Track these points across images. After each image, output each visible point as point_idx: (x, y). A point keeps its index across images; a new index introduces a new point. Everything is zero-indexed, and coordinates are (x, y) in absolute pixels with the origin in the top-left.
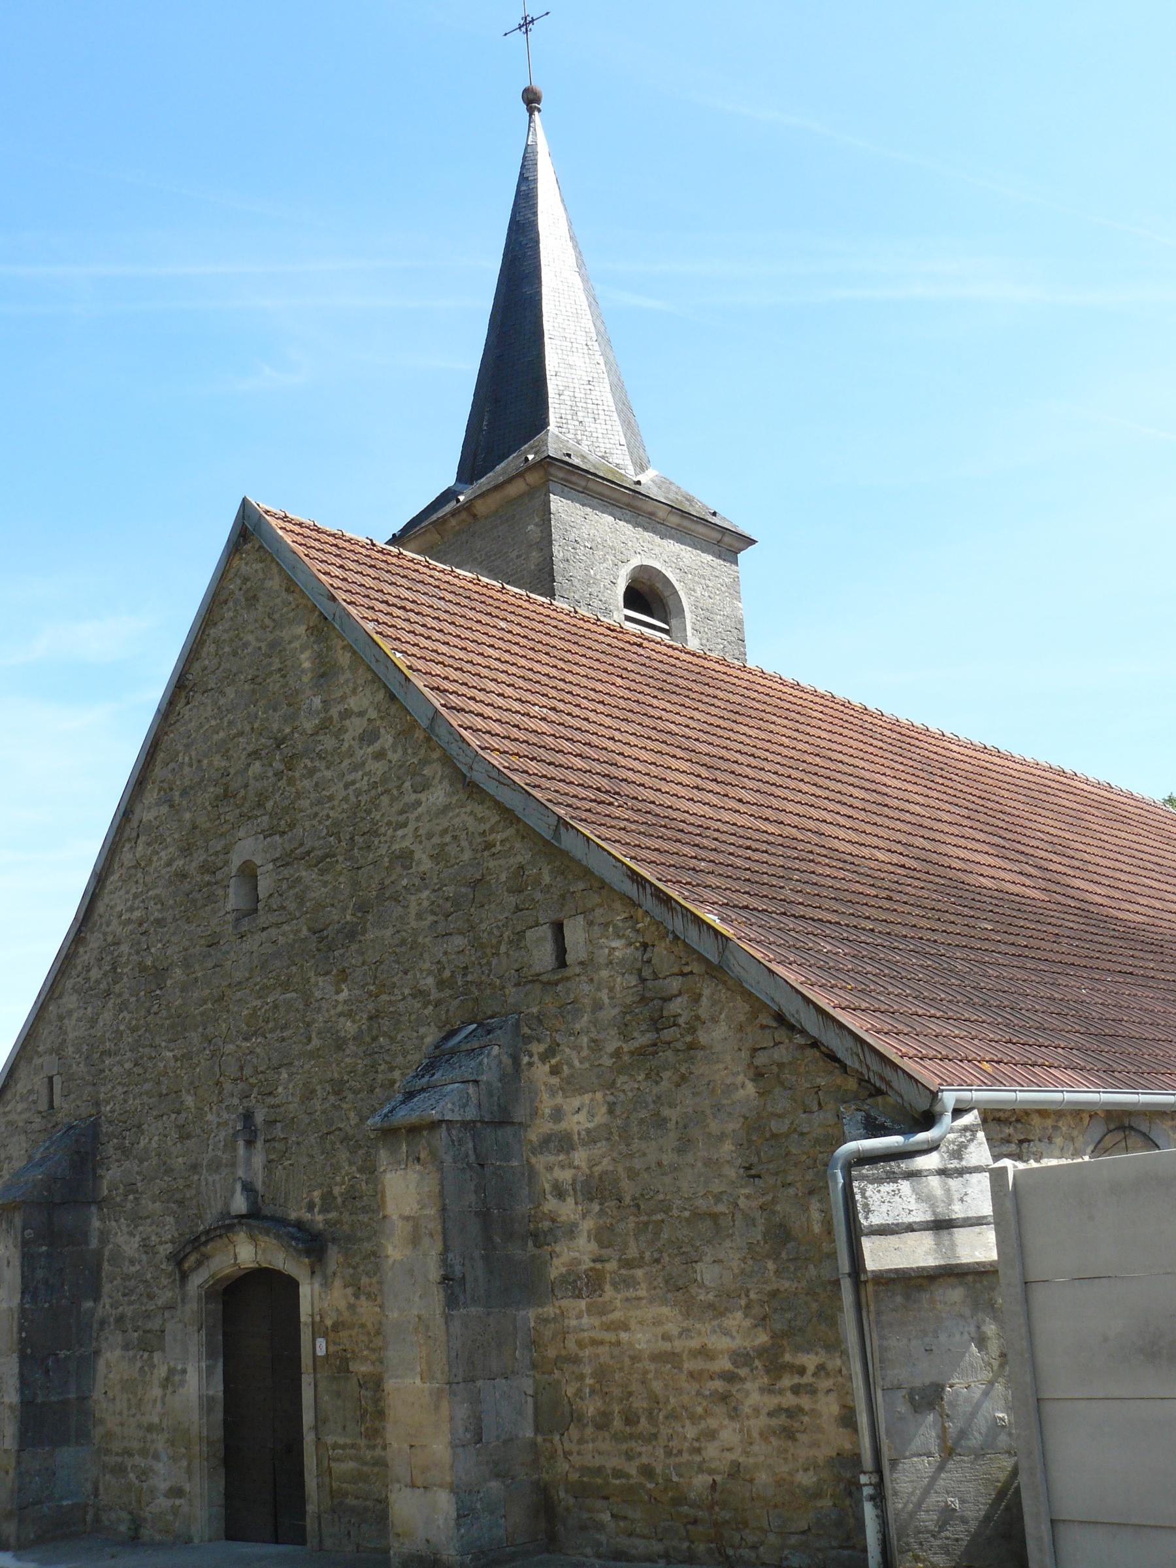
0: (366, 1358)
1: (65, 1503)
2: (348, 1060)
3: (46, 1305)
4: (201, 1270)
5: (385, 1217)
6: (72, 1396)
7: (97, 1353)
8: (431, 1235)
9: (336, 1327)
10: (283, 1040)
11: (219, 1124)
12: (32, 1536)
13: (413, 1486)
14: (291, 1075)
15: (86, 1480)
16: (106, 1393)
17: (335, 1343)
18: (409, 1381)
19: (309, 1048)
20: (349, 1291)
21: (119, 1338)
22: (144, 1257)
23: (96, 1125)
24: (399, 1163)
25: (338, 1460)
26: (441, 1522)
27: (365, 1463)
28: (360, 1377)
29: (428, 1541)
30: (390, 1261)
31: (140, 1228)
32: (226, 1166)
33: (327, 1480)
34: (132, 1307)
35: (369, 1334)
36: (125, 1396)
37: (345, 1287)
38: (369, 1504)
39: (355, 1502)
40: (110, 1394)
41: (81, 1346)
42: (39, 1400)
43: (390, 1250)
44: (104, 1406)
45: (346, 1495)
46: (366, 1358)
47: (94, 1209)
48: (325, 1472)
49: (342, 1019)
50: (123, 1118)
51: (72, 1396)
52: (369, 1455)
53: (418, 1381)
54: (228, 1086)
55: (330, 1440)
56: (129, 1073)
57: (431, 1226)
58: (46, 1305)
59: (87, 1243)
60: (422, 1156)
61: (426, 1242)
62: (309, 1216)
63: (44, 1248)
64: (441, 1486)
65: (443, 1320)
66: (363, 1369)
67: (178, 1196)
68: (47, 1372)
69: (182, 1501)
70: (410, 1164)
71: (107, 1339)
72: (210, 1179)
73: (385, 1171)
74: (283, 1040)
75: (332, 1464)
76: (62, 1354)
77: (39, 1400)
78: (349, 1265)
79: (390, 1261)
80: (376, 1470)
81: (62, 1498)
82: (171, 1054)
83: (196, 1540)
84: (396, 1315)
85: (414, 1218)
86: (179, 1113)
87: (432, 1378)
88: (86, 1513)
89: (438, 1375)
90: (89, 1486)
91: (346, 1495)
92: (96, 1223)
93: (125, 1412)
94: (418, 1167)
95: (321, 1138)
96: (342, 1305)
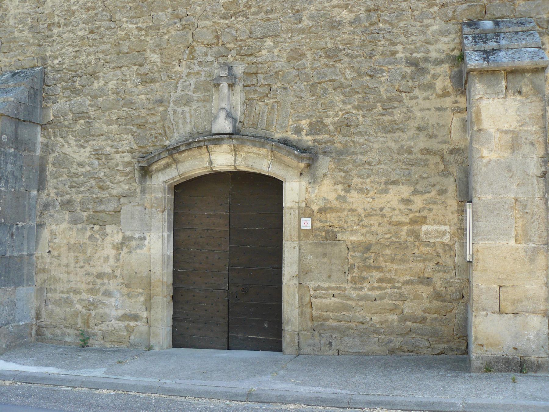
0: (357, 232)
1: (21, 323)
2: (346, 36)
3: (13, 190)
4: (167, 170)
5: (479, 130)
6: (25, 253)
7: (40, 226)
8: (532, 144)
9: (321, 211)
10: (268, 20)
11: (189, 74)
12: (4, 346)
13: (501, 312)
14: (276, 44)
15: (32, 308)
16: (49, 252)
17: (320, 221)
18: (501, 243)
19: (299, 26)
20: (340, 187)
21: (67, 216)
22: (96, 162)
23: (44, 73)
24: (498, 94)
25: (315, 297)
26: (532, 337)
27: (350, 298)
28: (348, 244)
29: (515, 349)
30: (485, 161)
31: (91, 143)
32: (197, 101)
33: (309, 310)
34: (80, 196)
35: (359, 215)
36: (72, 254)
37: (335, 184)
38: (353, 325)
39: (335, 324)
40: (55, 253)
41: (30, 220)
42: (8, 255)
43: (485, 153)
44: (48, 260)
45: (327, 319)
46: (357, 232)
47: (39, 128)
48: (305, 305)
49: (337, 9)
50: (73, 68)
51: (25, 253)
52: (354, 294)
53: (512, 242)
54: (200, 49)
55: (312, 284)
56: (83, 38)
57: (532, 138)
58: (13, 190)
59: (35, 151)
60: (524, 90)
61: (526, 149)
62: (295, 137)
63: (13, 150)
64: (534, 312)
65: (542, 202)
66: (353, 238)
67: (140, 121)
68: (12, 235)
69: (139, 323)
70: (508, 95)
71: (52, 216)
72: (179, 110)
73: (480, 99)
74: (268, 20)
75: (313, 300)
76: (20, 224)
77: (8, 255)
78: (340, 170)
79: (485, 161)
80: (361, 303)
81: (19, 321)
82: (134, 26)
83: (157, 348)
84: (489, 197)
85: (514, 131)
86: (141, 65)
87: (528, 239)
88: (32, 329)
89: (536, 238)
90: (33, 312)
91: (327, 319)
92: (40, 139)
93: (72, 265)
94: (519, 98)
95: (312, 85)
96: (332, 196)
